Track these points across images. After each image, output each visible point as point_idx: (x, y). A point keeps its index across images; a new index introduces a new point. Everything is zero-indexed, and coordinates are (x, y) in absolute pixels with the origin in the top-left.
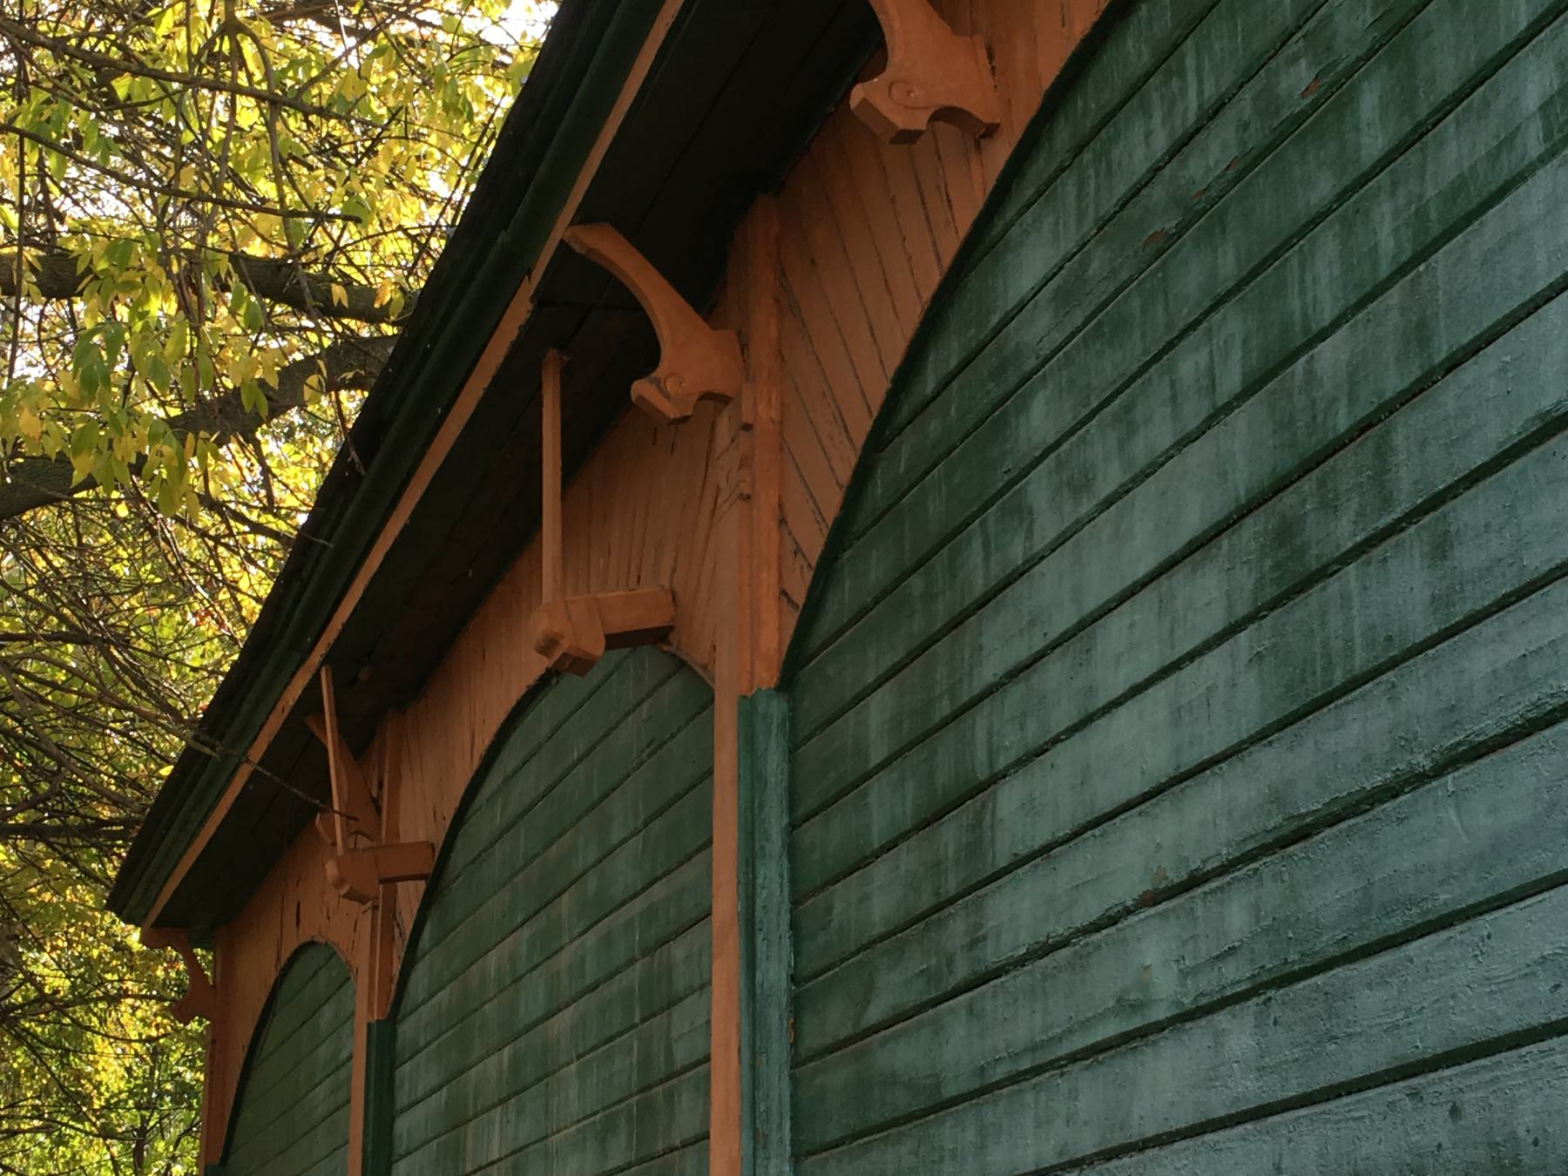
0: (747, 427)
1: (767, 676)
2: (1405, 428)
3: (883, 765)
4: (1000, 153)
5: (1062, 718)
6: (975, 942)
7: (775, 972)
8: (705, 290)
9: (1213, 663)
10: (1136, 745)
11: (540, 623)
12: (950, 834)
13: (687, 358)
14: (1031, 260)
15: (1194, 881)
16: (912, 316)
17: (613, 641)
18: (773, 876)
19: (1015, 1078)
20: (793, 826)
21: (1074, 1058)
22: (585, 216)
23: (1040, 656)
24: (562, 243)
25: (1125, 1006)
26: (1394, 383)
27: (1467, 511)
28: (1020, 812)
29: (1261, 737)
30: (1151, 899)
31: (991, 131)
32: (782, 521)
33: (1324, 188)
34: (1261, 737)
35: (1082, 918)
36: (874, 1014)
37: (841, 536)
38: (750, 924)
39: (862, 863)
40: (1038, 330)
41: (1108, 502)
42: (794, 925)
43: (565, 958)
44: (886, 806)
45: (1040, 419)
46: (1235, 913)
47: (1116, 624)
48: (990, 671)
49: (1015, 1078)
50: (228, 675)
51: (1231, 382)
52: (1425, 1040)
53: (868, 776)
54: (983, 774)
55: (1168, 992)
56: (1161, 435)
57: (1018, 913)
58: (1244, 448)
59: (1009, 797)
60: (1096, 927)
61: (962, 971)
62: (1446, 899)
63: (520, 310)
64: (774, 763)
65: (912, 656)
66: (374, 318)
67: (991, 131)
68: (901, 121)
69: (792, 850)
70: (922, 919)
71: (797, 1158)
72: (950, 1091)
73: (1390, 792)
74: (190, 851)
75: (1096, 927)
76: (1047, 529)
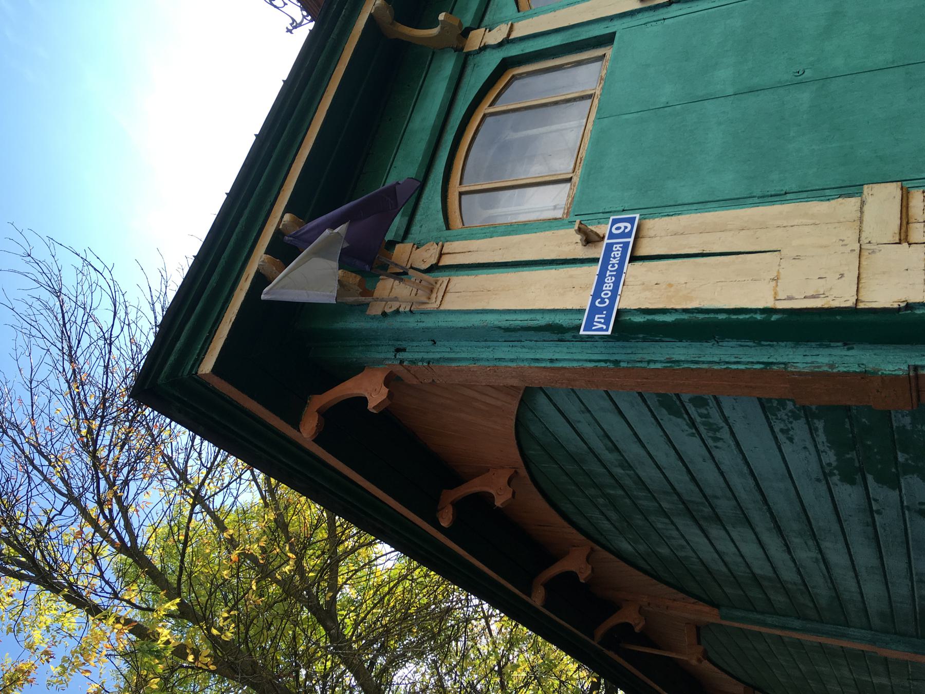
0: (649, 604)
1: (716, 611)
2: (686, 497)
3: (744, 592)
4: (598, 548)
5: (740, 560)
6: (795, 584)
7: (797, 623)
8: (612, 607)
9: (732, 534)
10: (750, 549)
11: (694, 662)
12: (765, 583)
13: (629, 616)
14: (625, 546)
15: (786, 545)
16: (630, 568)
17: (699, 643)
18: (769, 619)
19: (832, 582)
20: (757, 612)
21: (828, 572)
22: (593, 638)
23: (723, 561)
24: (600, 643)
25: (817, 561)
26: (676, 498)
27: (708, 492)
28: (761, 568)
29: (753, 529)
30: (789, 552)
31: (592, 549)
32: (674, 600)
33: (628, 501)
34: (753, 529)
35: (792, 565)
36: (811, 605)
37: (681, 590)
38: (783, 628)
39: (769, 600)
40: (642, 548)
41: (688, 544)
42: (783, 616)
43: (784, 663)
44: (755, 593)
45: (664, 551)
46: (796, 541)
47: (718, 547)
48: (724, 569)
49: (832, 582)
50: (501, 611)
51: (667, 521)
52: (833, 518)
53: (746, 595)
54: (751, 575)
55: (814, 554)
56: (675, 533)
57: (788, 575)
58: (683, 523)
59: (757, 571)
60: (795, 563)
61: (802, 587)
62: (799, 509)
63: (611, 654)
64: (738, 613)
65: (716, 581)
66: (599, 684)
67: (592, 549)
68: (589, 572)
69: (763, 613)
70: (787, 592)
71: (849, 626)
72: (834, 595)
73: (771, 514)
74: (409, 517)
75: (795, 563)
76: (691, 554)
